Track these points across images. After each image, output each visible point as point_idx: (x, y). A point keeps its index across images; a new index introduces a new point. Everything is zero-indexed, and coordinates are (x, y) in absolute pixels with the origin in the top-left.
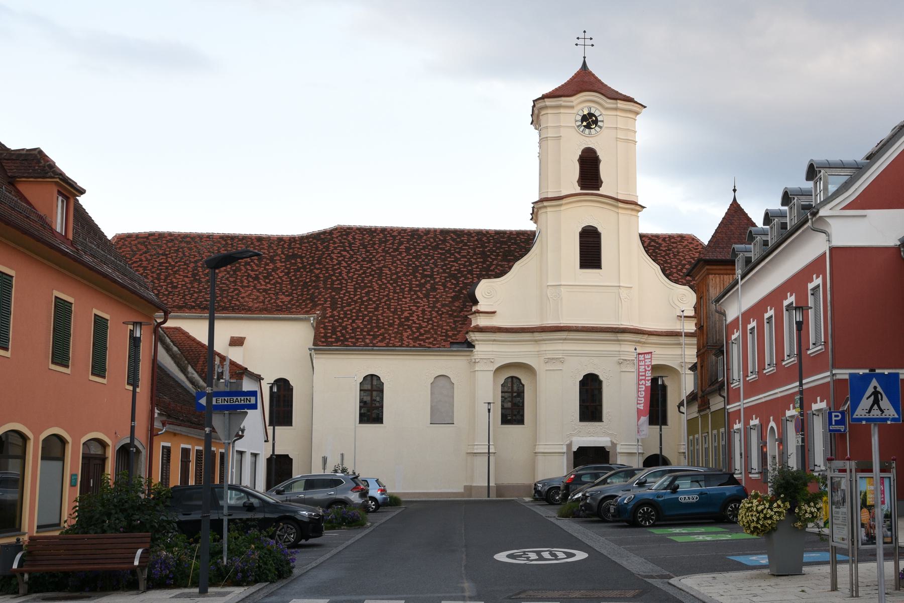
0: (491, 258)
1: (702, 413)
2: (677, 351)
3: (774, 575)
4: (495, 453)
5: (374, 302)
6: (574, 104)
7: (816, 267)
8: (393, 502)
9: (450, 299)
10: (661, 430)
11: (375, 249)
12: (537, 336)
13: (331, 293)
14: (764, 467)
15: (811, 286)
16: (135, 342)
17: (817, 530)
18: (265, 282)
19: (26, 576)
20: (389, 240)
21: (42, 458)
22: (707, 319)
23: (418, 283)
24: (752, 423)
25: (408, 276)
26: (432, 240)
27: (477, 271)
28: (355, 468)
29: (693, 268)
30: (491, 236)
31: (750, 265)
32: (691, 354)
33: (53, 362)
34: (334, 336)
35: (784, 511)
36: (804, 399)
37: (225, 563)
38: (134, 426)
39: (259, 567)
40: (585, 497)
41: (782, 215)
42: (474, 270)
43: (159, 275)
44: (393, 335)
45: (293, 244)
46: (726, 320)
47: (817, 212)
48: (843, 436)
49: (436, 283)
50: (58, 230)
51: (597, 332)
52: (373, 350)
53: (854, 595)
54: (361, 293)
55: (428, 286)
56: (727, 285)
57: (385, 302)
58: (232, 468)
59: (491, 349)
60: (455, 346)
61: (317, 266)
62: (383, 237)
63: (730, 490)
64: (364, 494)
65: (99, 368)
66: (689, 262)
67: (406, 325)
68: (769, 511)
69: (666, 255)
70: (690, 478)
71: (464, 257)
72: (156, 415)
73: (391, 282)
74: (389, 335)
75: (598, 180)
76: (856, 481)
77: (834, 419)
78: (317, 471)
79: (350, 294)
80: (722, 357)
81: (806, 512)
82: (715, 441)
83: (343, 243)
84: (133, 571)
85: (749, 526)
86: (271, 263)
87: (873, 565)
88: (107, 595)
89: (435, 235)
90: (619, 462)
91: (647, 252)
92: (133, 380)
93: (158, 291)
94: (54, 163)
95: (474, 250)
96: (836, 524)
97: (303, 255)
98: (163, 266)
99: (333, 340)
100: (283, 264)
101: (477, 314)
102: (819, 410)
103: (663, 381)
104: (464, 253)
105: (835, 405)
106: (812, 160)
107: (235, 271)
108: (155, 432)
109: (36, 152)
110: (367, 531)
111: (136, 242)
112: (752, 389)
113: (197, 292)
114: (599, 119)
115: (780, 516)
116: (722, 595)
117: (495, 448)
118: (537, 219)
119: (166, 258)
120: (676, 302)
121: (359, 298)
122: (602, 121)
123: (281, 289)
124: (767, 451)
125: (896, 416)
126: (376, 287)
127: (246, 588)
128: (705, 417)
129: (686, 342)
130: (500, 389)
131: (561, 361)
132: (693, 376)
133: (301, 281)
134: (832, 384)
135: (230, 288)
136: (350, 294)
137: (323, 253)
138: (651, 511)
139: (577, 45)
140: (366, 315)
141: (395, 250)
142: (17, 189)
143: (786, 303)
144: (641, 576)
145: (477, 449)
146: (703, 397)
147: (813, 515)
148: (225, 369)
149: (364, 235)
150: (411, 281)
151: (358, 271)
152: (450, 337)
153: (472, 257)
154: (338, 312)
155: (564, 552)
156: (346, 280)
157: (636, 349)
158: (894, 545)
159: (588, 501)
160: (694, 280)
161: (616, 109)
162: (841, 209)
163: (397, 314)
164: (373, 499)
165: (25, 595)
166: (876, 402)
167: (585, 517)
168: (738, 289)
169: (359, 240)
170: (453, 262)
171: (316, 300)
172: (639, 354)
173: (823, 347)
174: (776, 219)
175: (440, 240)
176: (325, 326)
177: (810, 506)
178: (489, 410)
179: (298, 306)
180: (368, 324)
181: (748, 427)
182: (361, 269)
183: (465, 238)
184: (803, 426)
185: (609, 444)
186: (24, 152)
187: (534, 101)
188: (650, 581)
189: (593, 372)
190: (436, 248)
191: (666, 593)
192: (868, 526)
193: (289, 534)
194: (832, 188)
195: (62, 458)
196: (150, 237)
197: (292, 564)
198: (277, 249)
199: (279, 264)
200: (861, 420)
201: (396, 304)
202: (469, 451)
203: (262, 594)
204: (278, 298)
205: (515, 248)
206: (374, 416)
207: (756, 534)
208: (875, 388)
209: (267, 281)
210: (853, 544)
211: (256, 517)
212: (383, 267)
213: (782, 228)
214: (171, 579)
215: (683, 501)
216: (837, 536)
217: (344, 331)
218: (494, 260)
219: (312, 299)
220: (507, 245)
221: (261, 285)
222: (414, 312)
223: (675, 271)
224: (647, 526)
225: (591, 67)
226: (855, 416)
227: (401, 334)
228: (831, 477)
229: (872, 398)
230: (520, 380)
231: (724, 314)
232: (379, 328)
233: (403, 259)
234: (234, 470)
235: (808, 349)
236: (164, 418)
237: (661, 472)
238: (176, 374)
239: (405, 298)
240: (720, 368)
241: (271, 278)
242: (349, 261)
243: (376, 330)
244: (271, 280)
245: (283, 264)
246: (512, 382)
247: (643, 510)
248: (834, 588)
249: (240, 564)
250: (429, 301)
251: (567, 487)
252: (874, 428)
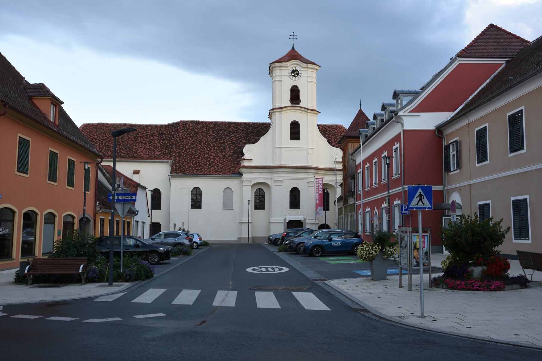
0: (250, 135)
1: (345, 205)
2: (334, 178)
3: (373, 280)
4: (251, 223)
5: (198, 155)
6: (288, 65)
7: (397, 139)
8: (205, 244)
9: (232, 154)
10: (326, 213)
11: (198, 131)
12: (271, 170)
13: (178, 150)
14: (372, 230)
15: (394, 148)
16: (87, 171)
17: (393, 259)
18: (149, 145)
19: (31, 276)
20: (205, 127)
21: (45, 223)
22: (347, 163)
23: (217, 146)
24: (367, 210)
25: (213, 143)
26: (224, 127)
27: (244, 141)
28: (189, 228)
29: (341, 140)
30: (251, 125)
31: (367, 138)
32: (339, 179)
33: (49, 180)
34: (180, 170)
35: (379, 251)
36: (391, 199)
37: (122, 271)
38: (85, 209)
39: (137, 273)
40: (290, 243)
41: (382, 115)
42: (243, 140)
43: (102, 142)
44: (206, 170)
45: (162, 128)
46: (356, 163)
47: (397, 114)
48: (408, 216)
49: (226, 146)
50: (51, 120)
51: (296, 168)
52: (197, 176)
53: (410, 290)
54: (192, 151)
55: (222, 148)
56: (356, 147)
57: (202, 155)
58: (133, 228)
59: (250, 176)
60: (234, 174)
61: (172, 138)
62: (202, 126)
63: (355, 241)
64: (191, 240)
65: (71, 183)
66: (339, 137)
67: (212, 165)
68: (371, 250)
69: (329, 134)
70: (338, 234)
71: (238, 134)
72: (97, 204)
73: (205, 145)
74: (205, 169)
75: (299, 100)
76: (412, 237)
77: (404, 208)
78: (172, 230)
79: (187, 151)
80: (354, 180)
81: (389, 251)
82: (350, 218)
83: (184, 128)
84: (79, 274)
85: (362, 257)
86: (152, 137)
87: (418, 276)
88: (68, 285)
89: (226, 125)
90: (307, 227)
91: (321, 133)
92: (86, 188)
93: (102, 149)
94: (49, 90)
95: (243, 131)
96: (402, 257)
97: (166, 133)
98: (104, 138)
99: (179, 171)
100: (157, 137)
101: (244, 160)
102: (397, 204)
103: (327, 191)
104: (238, 133)
105: (404, 202)
106: (395, 90)
107: (136, 141)
108: (97, 212)
109: (41, 85)
110: (191, 257)
111: (92, 127)
112: (367, 194)
113: (119, 150)
114: (300, 72)
115: (376, 253)
116: (348, 289)
117: (252, 220)
118: (271, 118)
119: (105, 135)
120: (334, 156)
121: (191, 153)
122: (301, 73)
123: (156, 149)
124: (373, 223)
125: (430, 206)
126: (199, 148)
127: (130, 283)
128: (346, 207)
129: (337, 173)
130: (254, 194)
131: (281, 181)
132: (341, 189)
133: (165, 145)
134: (403, 192)
135: (133, 148)
136: (187, 151)
137: (175, 133)
138: (320, 250)
139: (290, 38)
140: (195, 160)
141: (207, 131)
142: (33, 102)
143: (383, 155)
144: (312, 279)
145: (243, 221)
146: (345, 198)
147: (392, 252)
148: (121, 183)
149: (194, 124)
150: (214, 145)
151: (191, 140)
152: (232, 170)
153: (242, 135)
154: (182, 159)
155: (278, 268)
156: (185, 145)
157: (315, 176)
158: (429, 267)
159: (291, 244)
160: (342, 145)
161: (307, 68)
162: (408, 112)
163: (208, 160)
164: (196, 242)
165: (31, 285)
166: (421, 199)
167: (290, 252)
168: (361, 149)
169: (191, 127)
170: (233, 137)
171: (172, 153)
172: (316, 178)
173: (399, 175)
174: (379, 117)
175: (228, 127)
176: (176, 165)
177: (390, 248)
178: (249, 203)
179: (164, 156)
180: (195, 165)
181: (365, 212)
182: (192, 140)
183: (239, 126)
184: (390, 212)
185: (303, 219)
186: (36, 85)
187: (270, 64)
188: (315, 282)
189: (296, 187)
190: (225, 130)
191: (322, 288)
192: (417, 258)
193: (155, 258)
194: (404, 103)
195: (54, 223)
196: (98, 125)
197: (153, 272)
198: (155, 131)
199: (155, 138)
200: (413, 208)
201: (207, 155)
202: (240, 222)
203: (137, 286)
204: (155, 153)
205: (262, 131)
206: (198, 205)
207: (365, 261)
208: (420, 193)
209: (150, 145)
210: (410, 266)
211: (137, 250)
212: (202, 139)
213: (381, 121)
214: (97, 278)
215: (334, 245)
216: (402, 262)
217: (184, 168)
218: (252, 136)
219: (170, 153)
220: (258, 129)
221: (147, 147)
222: (215, 159)
223: (333, 141)
224: (318, 256)
226: (410, 206)
227: (210, 169)
228: (400, 235)
229: (419, 197)
230: (263, 190)
231: (355, 161)
232: (200, 166)
233: (211, 135)
234: (134, 229)
235: (393, 176)
236: (101, 206)
237: (325, 232)
238: (108, 186)
239: (212, 153)
240: (353, 185)
241: (152, 143)
242: (187, 136)
243: (198, 167)
244: (152, 145)
245: (157, 137)
246: (260, 191)
247: (316, 249)
248: (401, 286)
249: (128, 272)
250: (222, 154)
251: (283, 238)
252: (419, 212)
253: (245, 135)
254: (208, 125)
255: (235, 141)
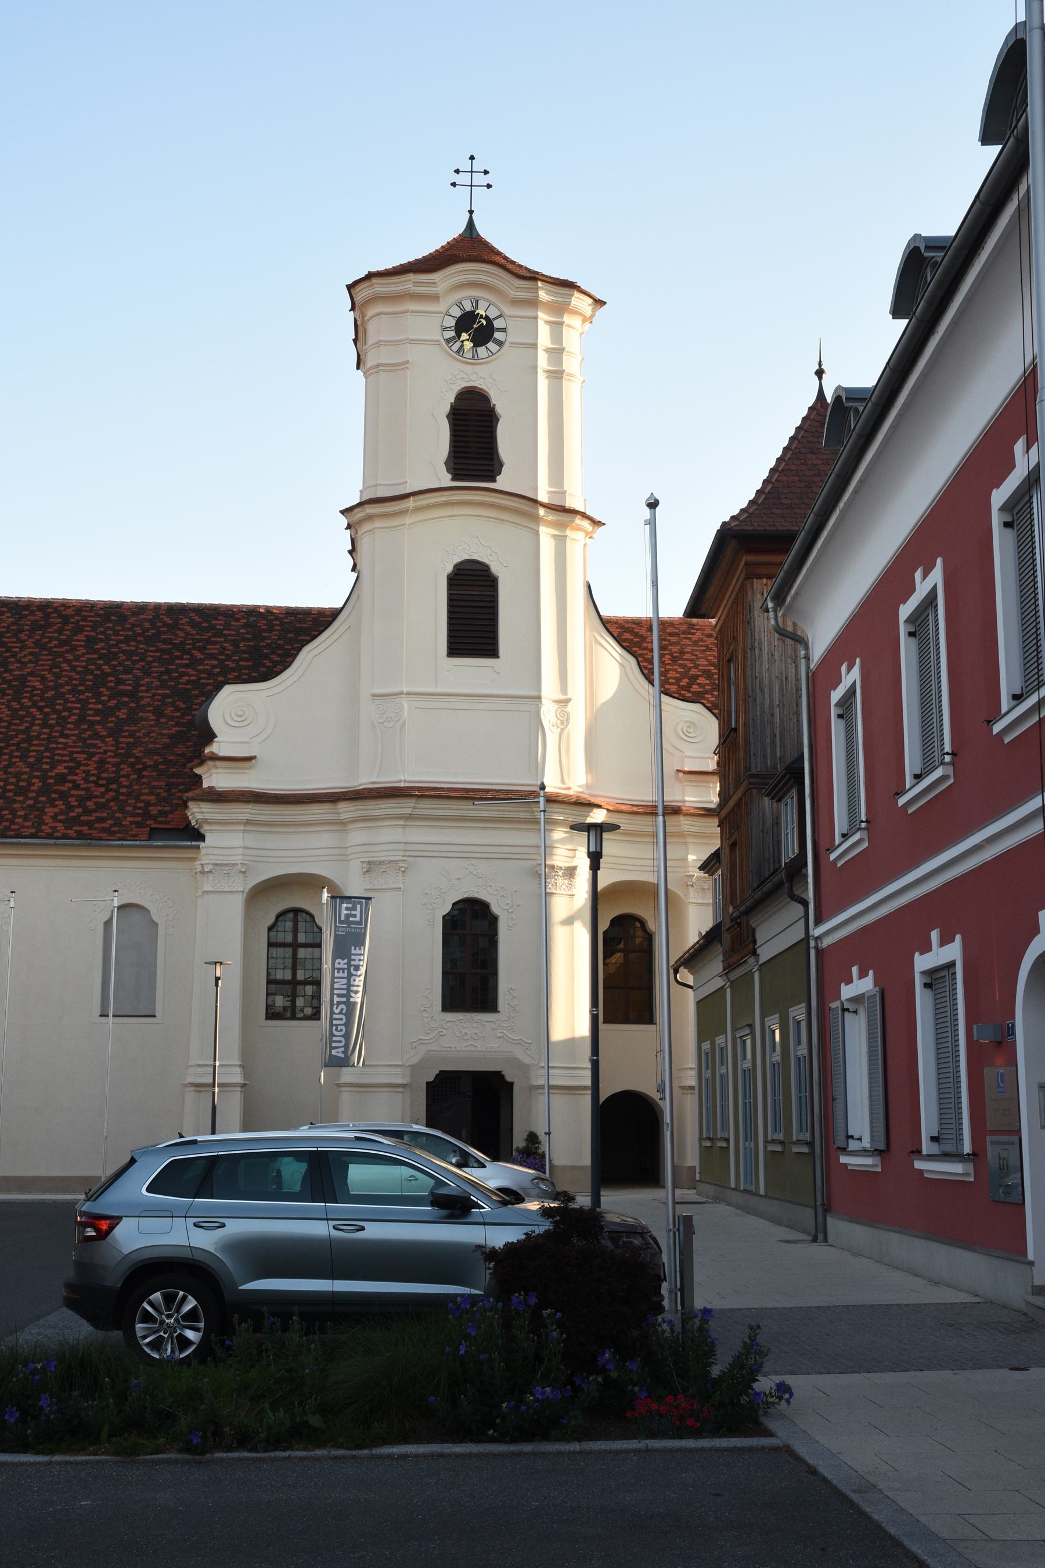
1: (734, 975)
6: (440, 289)
23: (100, 706)
25: (82, 692)
46: (807, 658)
55: (122, 714)
57: (18, 744)
66: (703, 671)
71: (212, 657)
75: (492, 459)
122: (504, 330)
139: (454, 184)
153: (229, 657)
170: (186, 666)
175: (165, 624)
183: (219, 623)
187: (350, 287)
189: (476, 896)
212: (32, 674)
222: (79, 764)
225: (484, 231)
231: (801, 641)
239: (67, 736)
253: (244, 660)
254: (72, 616)
255: (189, 687)
